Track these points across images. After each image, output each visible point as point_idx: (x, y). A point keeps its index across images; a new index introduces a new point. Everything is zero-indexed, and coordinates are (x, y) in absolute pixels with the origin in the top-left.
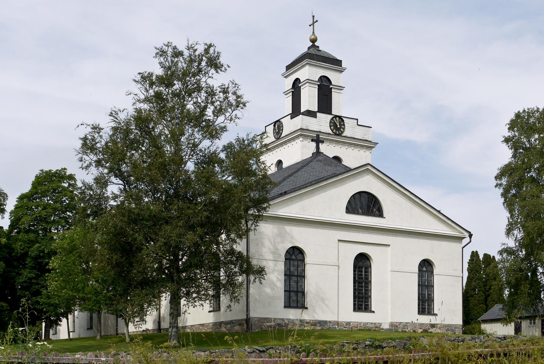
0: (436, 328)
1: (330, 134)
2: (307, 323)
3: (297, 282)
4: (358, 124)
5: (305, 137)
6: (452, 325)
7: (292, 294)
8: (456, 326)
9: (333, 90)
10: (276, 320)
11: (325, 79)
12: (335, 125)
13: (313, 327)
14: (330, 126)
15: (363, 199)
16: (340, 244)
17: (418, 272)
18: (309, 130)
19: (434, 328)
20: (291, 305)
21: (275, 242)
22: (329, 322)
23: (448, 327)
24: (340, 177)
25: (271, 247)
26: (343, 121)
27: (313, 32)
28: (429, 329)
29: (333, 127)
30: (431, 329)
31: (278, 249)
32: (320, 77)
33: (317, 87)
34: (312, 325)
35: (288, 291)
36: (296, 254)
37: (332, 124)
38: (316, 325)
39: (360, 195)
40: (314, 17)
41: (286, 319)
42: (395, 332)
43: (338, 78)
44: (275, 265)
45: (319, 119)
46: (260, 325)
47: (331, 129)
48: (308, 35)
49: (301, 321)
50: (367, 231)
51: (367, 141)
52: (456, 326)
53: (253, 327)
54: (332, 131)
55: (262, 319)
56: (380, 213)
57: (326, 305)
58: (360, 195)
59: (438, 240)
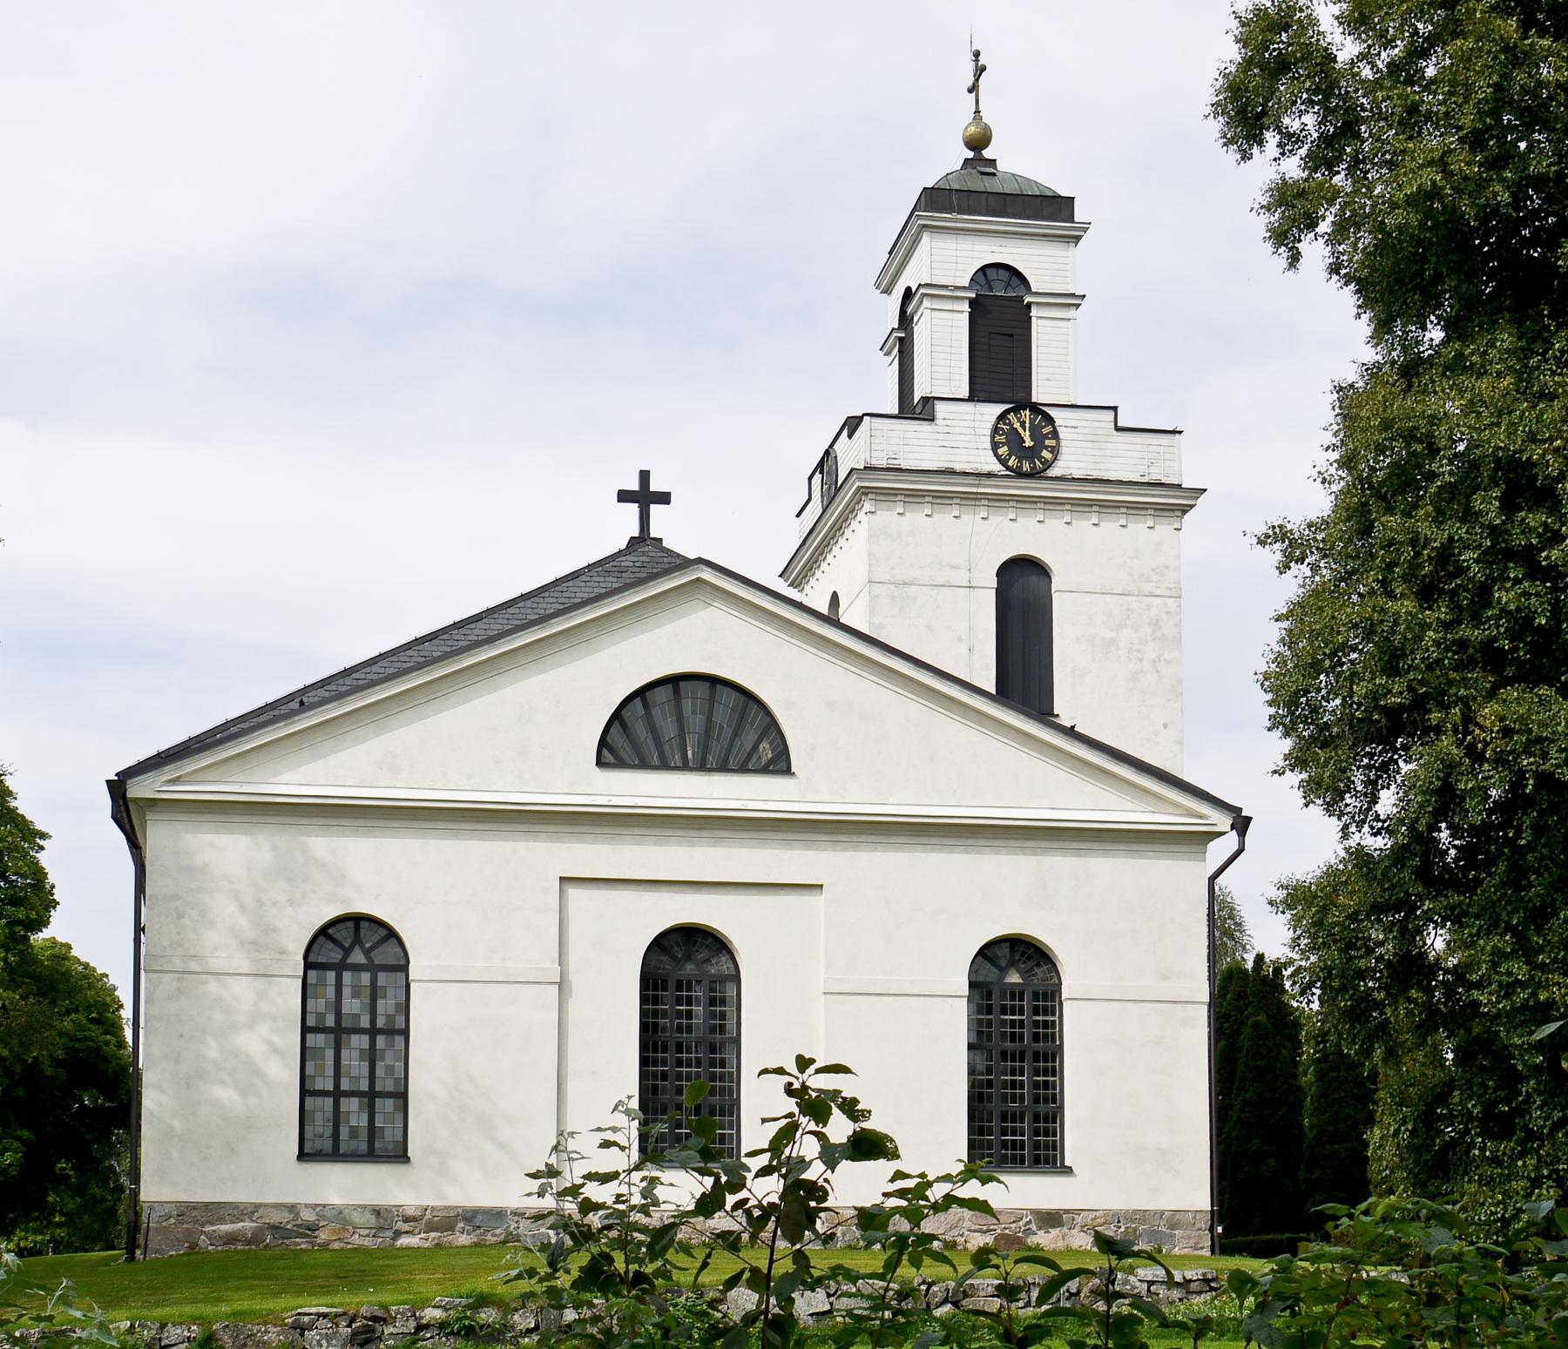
0: (1065, 1230)
1: (996, 476)
2: (407, 1220)
3: (372, 1056)
4: (1120, 424)
5: (1048, 507)
6: (1155, 1212)
7: (351, 1105)
8: (1175, 1220)
9: (1034, 312)
10: (261, 1212)
11: (1004, 274)
12: (1014, 440)
13: (432, 1235)
14: (995, 446)
15: (687, 704)
17: (965, 990)
18: (900, 470)
19: (1053, 1226)
21: (260, 903)
22: (514, 1213)
23: (1132, 1221)
24: (560, 623)
25: (244, 922)
26: (1050, 420)
27: (977, 112)
28: (1028, 1232)
29: (1006, 448)
30: (1041, 1233)
31: (275, 930)
32: (984, 269)
33: (966, 307)
34: (431, 1227)
36: (368, 945)
37: (1000, 438)
38: (452, 1228)
39: (677, 691)
40: (977, 54)
41: (307, 1206)
42: (847, 1251)
43: (1061, 266)
44: (261, 995)
45: (945, 422)
46: (188, 1233)
48: (960, 122)
49: (377, 1212)
50: (705, 833)
51: (1162, 485)
52: (1178, 1216)
53: (155, 1240)
54: (1003, 462)
55: (195, 1208)
56: (780, 764)
57: (500, 1145)
58: (677, 691)
59: (1077, 852)
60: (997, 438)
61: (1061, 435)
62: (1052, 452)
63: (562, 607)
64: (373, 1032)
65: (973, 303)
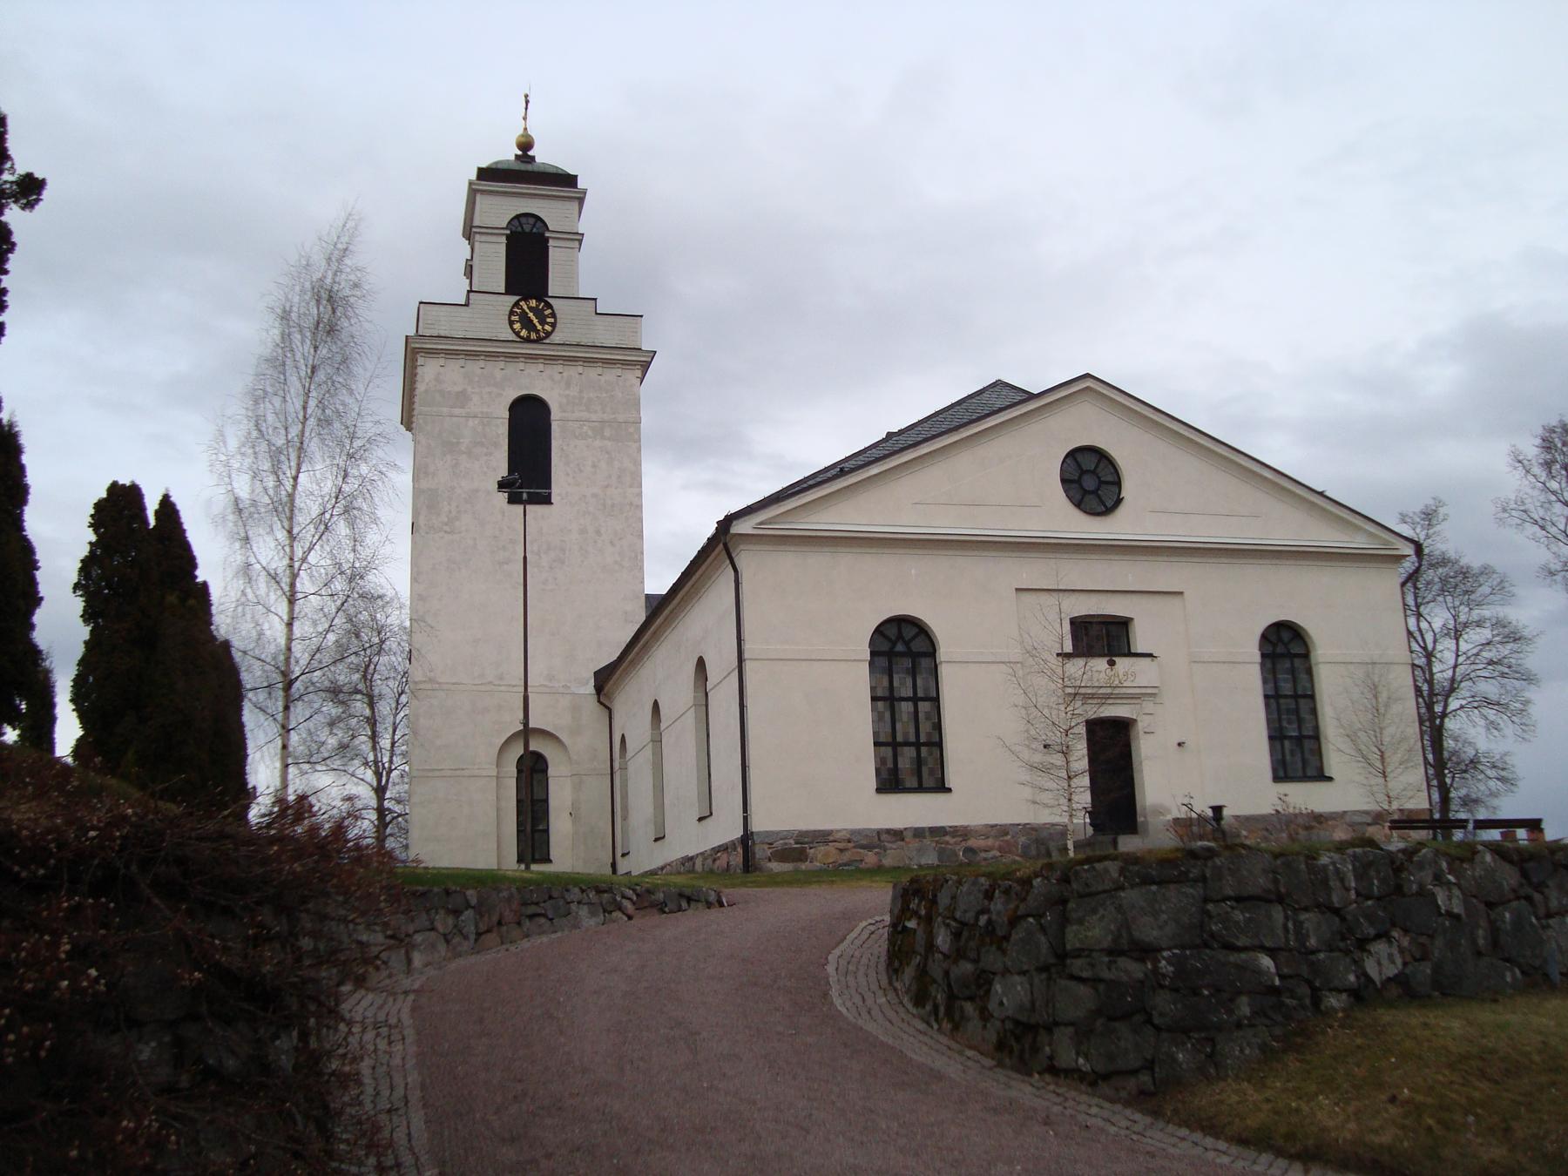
9: (551, 243)
16: (1020, 594)
20: (924, 786)
32: (518, 217)
33: (504, 239)
35: (887, 743)
47: (513, 330)
54: (517, 334)
60: (513, 318)
61: (558, 316)
62: (551, 326)
63: (887, 452)
64: (917, 745)
65: (508, 237)
